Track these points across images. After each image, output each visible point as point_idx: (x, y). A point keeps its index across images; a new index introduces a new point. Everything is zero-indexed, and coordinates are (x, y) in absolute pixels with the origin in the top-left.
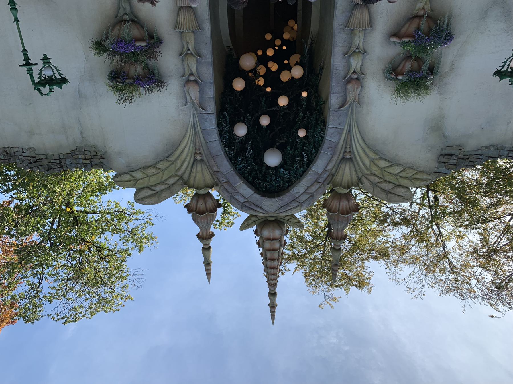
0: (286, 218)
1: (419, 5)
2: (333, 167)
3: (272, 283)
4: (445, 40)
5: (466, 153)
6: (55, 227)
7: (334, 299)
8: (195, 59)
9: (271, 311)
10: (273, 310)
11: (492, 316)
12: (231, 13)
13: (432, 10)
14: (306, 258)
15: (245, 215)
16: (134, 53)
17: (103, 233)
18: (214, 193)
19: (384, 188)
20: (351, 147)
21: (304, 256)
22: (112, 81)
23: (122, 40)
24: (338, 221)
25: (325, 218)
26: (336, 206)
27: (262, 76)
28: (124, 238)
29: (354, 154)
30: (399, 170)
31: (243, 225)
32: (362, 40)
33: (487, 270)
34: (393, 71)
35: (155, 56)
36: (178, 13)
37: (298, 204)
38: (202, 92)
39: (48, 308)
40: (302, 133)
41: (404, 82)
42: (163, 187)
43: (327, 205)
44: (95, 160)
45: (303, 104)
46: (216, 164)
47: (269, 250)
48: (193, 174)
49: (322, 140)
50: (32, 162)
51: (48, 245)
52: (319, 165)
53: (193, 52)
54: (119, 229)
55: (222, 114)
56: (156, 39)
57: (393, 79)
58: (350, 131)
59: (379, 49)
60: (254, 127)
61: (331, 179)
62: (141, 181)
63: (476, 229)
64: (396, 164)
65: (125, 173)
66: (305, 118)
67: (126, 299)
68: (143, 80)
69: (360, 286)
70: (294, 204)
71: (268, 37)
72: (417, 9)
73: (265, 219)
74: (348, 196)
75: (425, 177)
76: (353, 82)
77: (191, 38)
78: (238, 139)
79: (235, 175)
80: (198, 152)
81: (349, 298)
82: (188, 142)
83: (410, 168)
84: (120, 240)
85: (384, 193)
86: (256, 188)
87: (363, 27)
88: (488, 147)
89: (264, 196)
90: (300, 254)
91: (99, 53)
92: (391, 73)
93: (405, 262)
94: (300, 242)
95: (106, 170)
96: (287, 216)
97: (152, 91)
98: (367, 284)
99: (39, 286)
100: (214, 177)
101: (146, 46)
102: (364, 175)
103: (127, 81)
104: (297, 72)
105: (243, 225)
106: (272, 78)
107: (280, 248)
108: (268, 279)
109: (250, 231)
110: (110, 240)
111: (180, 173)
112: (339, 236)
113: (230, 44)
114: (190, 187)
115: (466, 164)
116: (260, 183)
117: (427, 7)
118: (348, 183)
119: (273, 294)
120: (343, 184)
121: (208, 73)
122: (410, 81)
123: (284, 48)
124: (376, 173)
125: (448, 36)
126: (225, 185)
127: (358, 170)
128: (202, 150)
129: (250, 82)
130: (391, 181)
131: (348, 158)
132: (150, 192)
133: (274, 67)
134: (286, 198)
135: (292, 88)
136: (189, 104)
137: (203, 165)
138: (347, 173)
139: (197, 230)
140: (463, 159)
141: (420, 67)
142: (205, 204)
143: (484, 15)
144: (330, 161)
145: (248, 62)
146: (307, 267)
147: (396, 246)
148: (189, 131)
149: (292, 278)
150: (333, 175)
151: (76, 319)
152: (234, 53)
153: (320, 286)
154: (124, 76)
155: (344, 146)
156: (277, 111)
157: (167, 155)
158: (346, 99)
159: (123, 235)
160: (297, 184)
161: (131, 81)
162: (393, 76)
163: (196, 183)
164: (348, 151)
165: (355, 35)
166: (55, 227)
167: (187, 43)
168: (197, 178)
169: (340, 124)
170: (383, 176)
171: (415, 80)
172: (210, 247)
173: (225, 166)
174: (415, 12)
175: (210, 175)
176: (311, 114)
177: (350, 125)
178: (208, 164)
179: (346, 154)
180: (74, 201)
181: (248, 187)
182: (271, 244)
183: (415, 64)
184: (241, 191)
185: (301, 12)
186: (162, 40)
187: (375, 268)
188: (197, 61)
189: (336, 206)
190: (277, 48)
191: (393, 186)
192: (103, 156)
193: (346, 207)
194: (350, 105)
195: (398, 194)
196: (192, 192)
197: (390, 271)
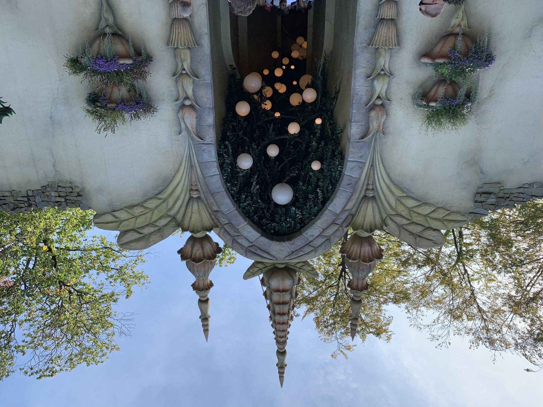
0: (297, 265)
1: (455, 21)
2: (353, 207)
3: (281, 340)
4: (486, 61)
5: (505, 191)
6: (31, 266)
7: (349, 348)
8: (191, 81)
9: (279, 372)
10: (281, 371)
11: (528, 370)
12: (234, 19)
13: (469, 27)
14: (317, 301)
15: (250, 262)
16: (117, 73)
17: (88, 272)
18: (214, 235)
19: (412, 231)
20: (374, 183)
21: (315, 298)
22: (89, 105)
23: (102, 57)
24: (359, 268)
26: (356, 252)
27: (269, 99)
28: (112, 277)
30: (430, 211)
32: (388, 60)
34: (423, 96)
35: (143, 75)
37: (312, 248)
38: (199, 119)
39: (19, 359)
41: (438, 110)
42: (152, 229)
45: (316, 133)
46: (216, 202)
47: (278, 303)
48: (189, 214)
49: (341, 175)
51: (23, 288)
52: (338, 204)
53: (188, 72)
54: (106, 267)
55: (223, 143)
56: (144, 56)
57: (424, 106)
58: (372, 165)
59: (407, 71)
60: (261, 158)
61: (351, 219)
63: (511, 272)
64: (426, 204)
65: (107, 213)
66: (319, 148)
67: (112, 349)
70: (307, 249)
71: (275, 55)
72: (452, 25)
74: (370, 240)
76: (378, 109)
77: (186, 55)
78: (242, 172)
79: (238, 215)
80: (194, 188)
81: (366, 345)
82: (182, 176)
83: (442, 208)
84: (107, 279)
85: (412, 237)
86: (262, 229)
87: (389, 45)
88: (531, 185)
89: (272, 239)
90: (311, 296)
91: (75, 72)
92: (422, 99)
93: (427, 305)
94: (311, 283)
95: (85, 208)
96: (299, 262)
98: (386, 331)
99: (10, 334)
100: (213, 217)
101: (131, 64)
102: (389, 216)
103: (109, 105)
104: (310, 96)
105: (248, 273)
106: (280, 101)
107: (290, 301)
108: (277, 335)
109: (256, 280)
110: (93, 280)
111: (172, 213)
112: (360, 286)
114: (184, 230)
115: (505, 204)
116: (267, 224)
117: (464, 23)
118: (371, 226)
119: (281, 353)
120: (365, 227)
121: (207, 97)
122: (445, 108)
123: (293, 67)
124: (403, 213)
125: (490, 57)
126: (226, 227)
127: (382, 210)
128: (199, 186)
129: (255, 106)
130: (421, 223)
131: (370, 196)
132: (137, 236)
133: (282, 88)
134: (298, 242)
135: (304, 113)
136: (184, 133)
137: (200, 204)
139: (192, 279)
140: (502, 198)
141: (455, 93)
142: (203, 249)
143: (529, 33)
144: (349, 200)
146: (318, 311)
147: (416, 287)
148: (183, 164)
149: (303, 325)
150: (353, 216)
151: (53, 373)
152: (237, 72)
153: (333, 334)
154: (105, 100)
155: (366, 182)
156: (286, 139)
157: (157, 192)
158: (368, 128)
161: (113, 105)
163: (192, 225)
164: (371, 188)
166: (31, 266)
167: (182, 62)
168: (193, 219)
169: (361, 157)
170: (411, 217)
171: (450, 108)
172: (208, 299)
173: (227, 205)
175: (208, 215)
176: (326, 144)
178: (206, 203)
179: (368, 192)
180: (54, 237)
181: (254, 228)
182: (280, 295)
184: (245, 233)
185: (312, 28)
186: (152, 58)
188: (194, 82)
189: (356, 252)
190: (284, 67)
192: (80, 193)
193: (368, 253)
194: (373, 135)
196: (188, 234)
197: (411, 316)
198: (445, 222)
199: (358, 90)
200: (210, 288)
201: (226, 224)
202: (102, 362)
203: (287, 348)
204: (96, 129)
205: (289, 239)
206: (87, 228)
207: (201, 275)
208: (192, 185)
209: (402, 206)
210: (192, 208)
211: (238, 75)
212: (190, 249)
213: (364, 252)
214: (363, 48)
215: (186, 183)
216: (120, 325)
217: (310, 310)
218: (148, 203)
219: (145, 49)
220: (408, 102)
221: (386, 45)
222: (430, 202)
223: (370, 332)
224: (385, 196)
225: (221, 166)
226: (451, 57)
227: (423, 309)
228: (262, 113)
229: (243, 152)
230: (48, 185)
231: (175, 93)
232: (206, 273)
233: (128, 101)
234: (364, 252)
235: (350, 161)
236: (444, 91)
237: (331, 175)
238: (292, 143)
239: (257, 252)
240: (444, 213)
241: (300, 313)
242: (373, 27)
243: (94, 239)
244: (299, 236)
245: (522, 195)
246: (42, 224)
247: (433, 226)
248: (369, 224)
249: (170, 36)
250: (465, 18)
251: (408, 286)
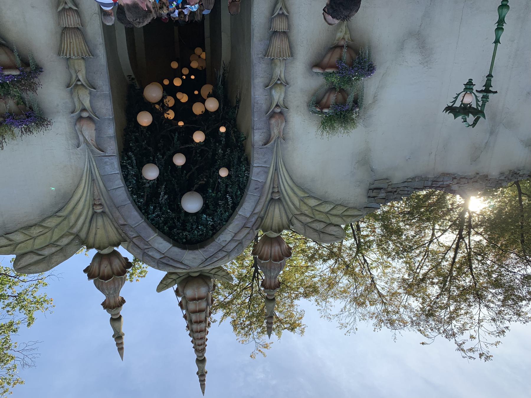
0: (211, 272)
1: (340, 35)
3: (200, 347)
4: (368, 70)
5: (393, 186)
7: (266, 346)
8: (88, 92)
10: (202, 379)
11: (423, 343)
13: (352, 41)
14: (233, 304)
15: (163, 274)
18: (122, 250)
19: (316, 228)
20: (279, 186)
24: (271, 268)
25: (251, 258)
26: (267, 252)
27: (171, 108)
28: (8, 305)
29: (282, 193)
30: (330, 208)
31: (161, 286)
33: (414, 297)
35: (33, 87)
36: (62, 35)
37: (225, 254)
38: (98, 130)
40: (224, 173)
41: (330, 116)
42: (54, 250)
43: (257, 251)
45: (221, 141)
47: (195, 312)
48: (93, 231)
49: (248, 180)
52: (246, 209)
53: (84, 83)
55: (126, 154)
56: (32, 67)
57: (319, 113)
58: (276, 169)
59: (301, 81)
60: (167, 167)
61: (260, 222)
62: (22, 245)
63: (403, 258)
64: (326, 202)
67: (15, 384)
68: (17, 118)
69: (292, 329)
70: (221, 255)
71: (175, 65)
72: (337, 38)
73: (187, 276)
74: (279, 240)
77: (81, 65)
78: (148, 183)
79: (147, 227)
81: (283, 341)
82: (83, 191)
83: (340, 205)
85: (315, 233)
88: (413, 179)
89: (184, 248)
90: (227, 300)
92: (316, 106)
93: (334, 296)
94: (225, 288)
97: (31, 132)
98: (299, 325)
100: (120, 231)
101: (19, 75)
102: (294, 215)
104: (212, 105)
105: (161, 286)
106: (183, 111)
108: (195, 344)
109: (171, 291)
111: (75, 230)
112: (273, 284)
113: (131, 73)
116: (179, 234)
117: (347, 37)
118: (279, 226)
119: (201, 361)
120: (273, 228)
121: (106, 108)
123: (193, 77)
124: (307, 212)
125: (371, 67)
126: (134, 240)
127: (288, 211)
128: (103, 201)
129: (157, 116)
130: (323, 220)
131: (276, 199)
133: (184, 98)
134: (211, 248)
135: (207, 122)
136: (83, 146)
137: (105, 218)
138: (277, 215)
139: (103, 298)
140: (391, 192)
141: (345, 100)
143: (401, 46)
145: (153, 93)
146: (235, 314)
147: (323, 281)
148: (84, 178)
149: (220, 329)
150: (262, 219)
155: (272, 186)
156: (192, 147)
157: (56, 210)
158: (270, 135)
159: (6, 302)
160: (223, 231)
162: (318, 110)
163: (97, 242)
164: (276, 191)
165: (276, 65)
167: (76, 72)
168: (98, 236)
169: (265, 162)
170: (314, 215)
171: (341, 113)
172: (121, 316)
173: (134, 217)
174: (336, 42)
175: (115, 230)
177: (276, 162)
179: (274, 195)
181: (165, 239)
182: (196, 304)
183: (340, 97)
184: (156, 246)
186: (42, 68)
187: (303, 305)
188: (90, 93)
189: (267, 252)
190: (184, 77)
191: (325, 225)
193: (278, 252)
195: (330, 233)
196: (94, 252)
197: (321, 308)
203: (205, 355)
205: (202, 247)
207: (111, 292)
208: (94, 199)
209: (305, 206)
210: (96, 223)
211: (138, 85)
213: (275, 252)
215: (88, 197)
217: (226, 315)
218: (46, 222)
219: (33, 59)
225: (126, 178)
227: (331, 300)
229: (148, 162)
232: (117, 290)
234: (275, 252)
235: (255, 167)
236: (334, 98)
237: (239, 181)
238: (198, 151)
244: (212, 242)
245: (406, 189)
250: (348, 33)
251: (316, 280)
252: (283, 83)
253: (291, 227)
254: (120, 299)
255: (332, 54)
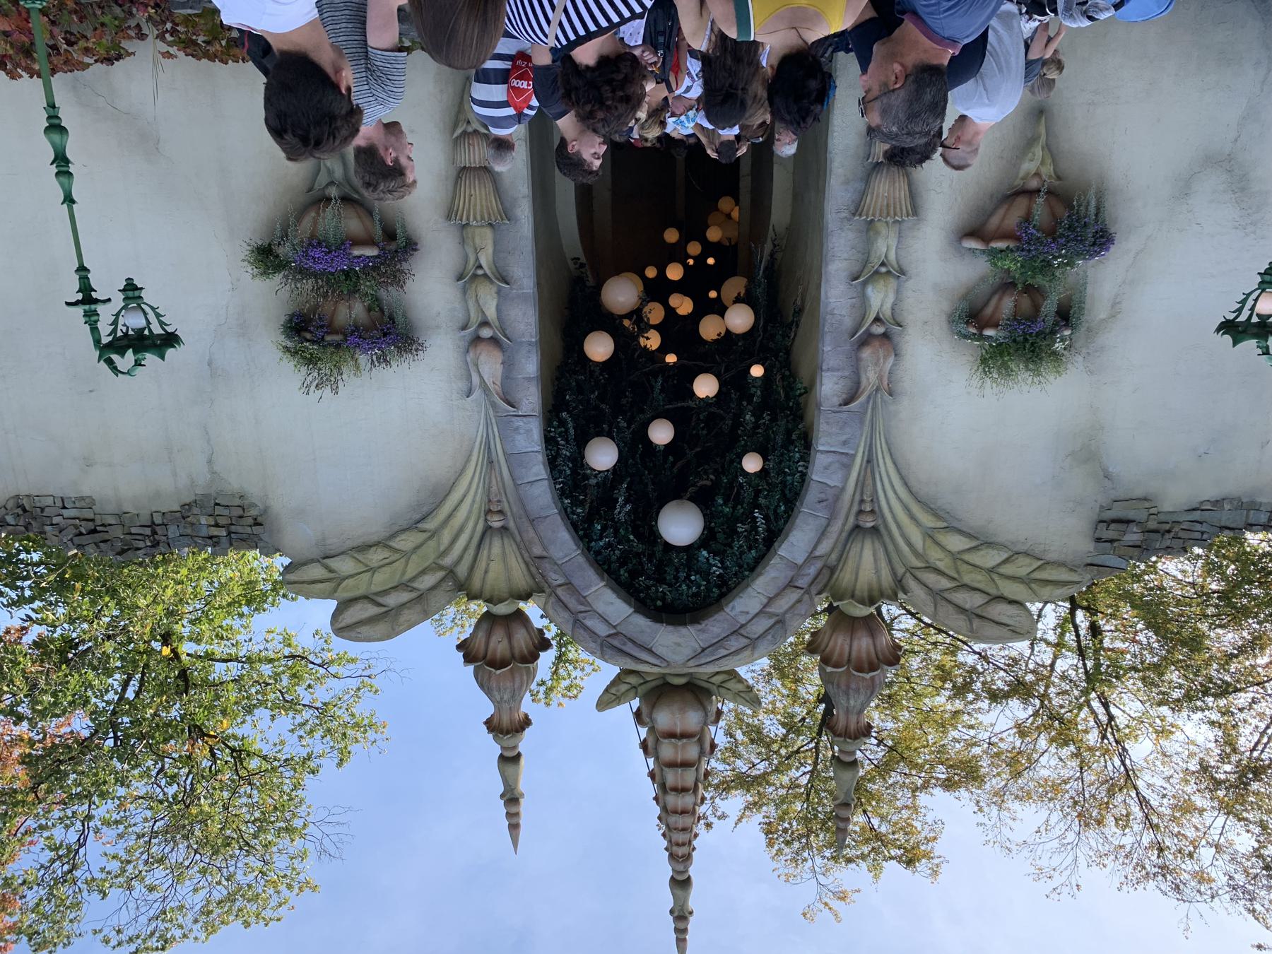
0: (714, 680)
1: (1028, 166)
2: (832, 550)
3: (680, 854)
4: (1094, 244)
5: (1162, 518)
6: (130, 694)
8: (494, 289)
10: (681, 926)
11: (1259, 947)
13: (1059, 178)
15: (610, 671)
16: (347, 274)
18: (532, 609)
21: (762, 779)
22: (288, 337)
23: (319, 244)
24: (848, 687)
26: (842, 648)
27: (655, 327)
30: (998, 559)
31: (606, 698)
34: (971, 317)
37: (744, 642)
38: (509, 366)
39: (94, 910)
40: (752, 464)
41: (1001, 344)
42: (405, 596)
43: (819, 646)
44: (239, 529)
46: (540, 538)
47: (672, 765)
48: (482, 564)
49: (803, 481)
50: (84, 531)
52: (798, 543)
53: (488, 272)
55: (557, 416)
56: (401, 241)
57: (972, 337)
59: (934, 265)
60: (635, 448)
61: (827, 578)
62: (350, 582)
64: (989, 544)
65: (312, 561)
69: (910, 863)
70: (735, 644)
71: (671, 236)
72: (1022, 174)
73: (660, 682)
74: (873, 624)
75: (1064, 575)
77: (485, 239)
78: (596, 476)
79: (586, 566)
80: (495, 508)
82: (471, 483)
83: (1026, 554)
84: (292, 731)
85: (963, 617)
86: (638, 599)
88: (1218, 503)
90: (754, 773)
91: (264, 273)
92: (967, 323)
94: (752, 741)
95: (267, 552)
96: (718, 673)
98: (927, 856)
99: (77, 852)
100: (533, 569)
102: (910, 570)
103: (328, 338)
104: (740, 319)
105: (606, 698)
106: (679, 332)
108: (670, 841)
109: (624, 712)
110: (264, 732)
111: (448, 561)
112: (853, 726)
113: (579, 253)
114: (472, 597)
115: (1164, 546)
116: (648, 588)
117: (1047, 170)
118: (870, 590)
119: (681, 883)
120: (857, 592)
121: (525, 321)
122: (1014, 341)
123: (711, 261)
124: (940, 565)
125: (1102, 237)
126: (559, 591)
128: (506, 505)
131: (867, 526)
132: (372, 610)
133: (683, 305)
134: (715, 626)
135: (728, 356)
136: (477, 393)
138: (866, 565)
141: (1037, 308)
143: (1184, 188)
144: (823, 534)
145: (621, 294)
147: (998, 755)
148: (474, 458)
149: (732, 836)
150: (832, 570)
154: (322, 327)
155: (857, 498)
156: (692, 409)
157: (418, 517)
158: (858, 383)
160: (742, 590)
161: (338, 338)
163: (488, 588)
164: (868, 509)
165: (878, 233)
166: (130, 694)
168: (491, 575)
169: (845, 443)
170: (958, 572)
171: (1026, 340)
172: (519, 755)
173: (562, 543)
175: (523, 566)
176: (774, 419)
178: (518, 539)
179: (862, 517)
180: (183, 628)
181: (619, 596)
182: (676, 747)
183: (1026, 302)
184: (600, 607)
186: (416, 244)
187: (946, 811)
188: (499, 292)
190: (691, 262)
191: (985, 598)
192: (259, 519)
193: (868, 653)
194: (869, 397)
195: (996, 619)
196: (478, 607)
197: (986, 820)
198: (1033, 585)
199: (833, 305)
200: (523, 729)
201: (560, 586)
202: (279, 920)
203: (692, 871)
204: (300, 385)
205: (695, 621)
206: (256, 609)
207: (506, 697)
208: (490, 501)
209: (938, 549)
210: (490, 549)
211: (590, 278)
212: (483, 640)
213: (859, 651)
214: (842, 220)
215: (478, 498)
216: (319, 835)
217: (750, 807)
219: (404, 226)
220: (940, 328)
221: (888, 214)
222: (999, 540)
223: (892, 858)
224: (899, 527)
226: (1021, 238)
227: (1015, 806)
228: (640, 356)
229: (599, 434)
230: (195, 501)
231: (460, 315)
232: (516, 697)
233: (366, 330)
234: (859, 651)
235: (822, 452)
236: (1012, 305)
237: (784, 483)
238: (701, 417)
239: (624, 648)
240: (1031, 565)
241: (727, 812)
242: (861, 179)
243: (270, 637)
244: (716, 612)
245: (1198, 527)
246: (169, 592)
247: (1006, 594)
248: (866, 587)
249: (453, 203)
250: (1049, 161)
251: (976, 751)
252: (895, 272)
253: (901, 595)
254: (522, 716)
255: (1008, 209)
